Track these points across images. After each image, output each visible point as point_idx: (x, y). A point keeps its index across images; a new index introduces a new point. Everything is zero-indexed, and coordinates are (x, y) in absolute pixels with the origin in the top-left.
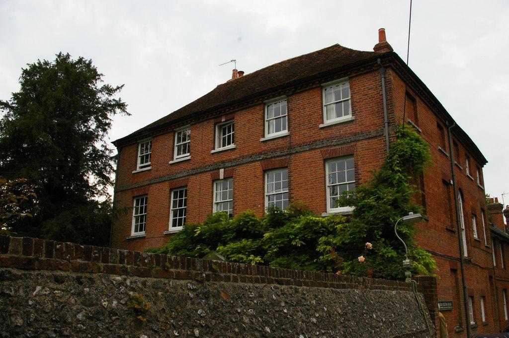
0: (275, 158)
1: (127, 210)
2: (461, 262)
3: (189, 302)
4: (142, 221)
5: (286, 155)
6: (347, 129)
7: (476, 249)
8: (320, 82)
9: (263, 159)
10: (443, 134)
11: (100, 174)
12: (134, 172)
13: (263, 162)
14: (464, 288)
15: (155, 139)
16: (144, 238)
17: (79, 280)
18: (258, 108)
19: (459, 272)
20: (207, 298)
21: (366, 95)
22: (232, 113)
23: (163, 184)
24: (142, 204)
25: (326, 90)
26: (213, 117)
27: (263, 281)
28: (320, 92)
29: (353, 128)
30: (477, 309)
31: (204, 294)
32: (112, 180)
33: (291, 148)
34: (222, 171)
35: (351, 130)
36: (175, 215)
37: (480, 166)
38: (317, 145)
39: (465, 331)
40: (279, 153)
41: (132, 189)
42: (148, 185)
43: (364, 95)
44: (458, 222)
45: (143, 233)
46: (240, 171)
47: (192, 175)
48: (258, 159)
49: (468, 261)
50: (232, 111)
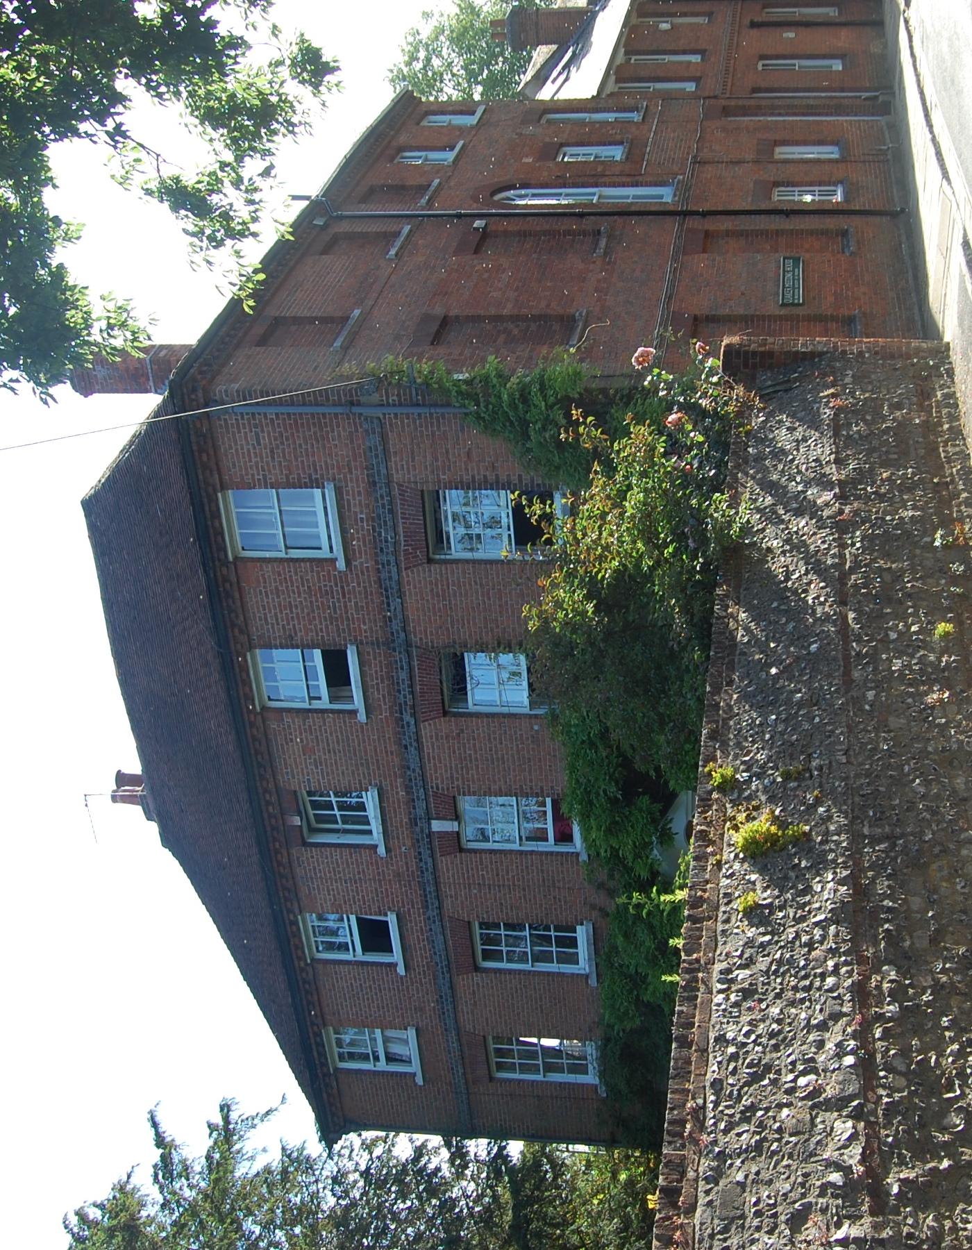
8: (225, 562)
9: (414, 715)
21: (272, 452)
34: (437, 826)
35: (359, 493)
38: (390, 578)
40: (403, 675)
41: (466, 1083)
43: (273, 458)
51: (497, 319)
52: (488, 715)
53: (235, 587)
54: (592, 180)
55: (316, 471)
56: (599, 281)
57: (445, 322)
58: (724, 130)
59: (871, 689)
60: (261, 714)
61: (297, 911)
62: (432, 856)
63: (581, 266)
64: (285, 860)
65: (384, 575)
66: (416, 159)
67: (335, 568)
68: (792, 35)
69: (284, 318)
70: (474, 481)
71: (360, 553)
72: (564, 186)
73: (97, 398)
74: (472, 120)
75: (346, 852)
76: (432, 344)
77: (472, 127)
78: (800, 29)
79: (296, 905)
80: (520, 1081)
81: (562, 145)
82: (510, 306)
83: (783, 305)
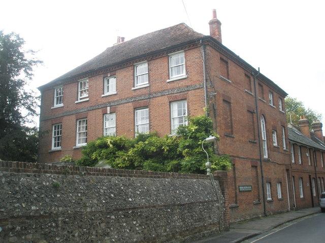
0: (142, 101)
1: (49, 132)
3: (76, 184)
4: (59, 140)
7: (275, 153)
9: (134, 101)
11: (29, 108)
12: (52, 108)
14: (263, 177)
17: (35, 176)
18: (130, 68)
19: (259, 168)
20: (84, 182)
24: (58, 129)
27: (111, 175)
29: (187, 83)
31: (83, 180)
32: (37, 112)
34: (108, 108)
36: (55, 141)
37: (282, 97)
39: (262, 204)
40: (143, 98)
44: (259, 135)
45: (59, 148)
49: (267, 161)
51: (231, 116)
57: (229, 103)
63: (246, 136)
66: (271, 97)
73: (209, 26)
74: (281, 110)
76: (248, 111)
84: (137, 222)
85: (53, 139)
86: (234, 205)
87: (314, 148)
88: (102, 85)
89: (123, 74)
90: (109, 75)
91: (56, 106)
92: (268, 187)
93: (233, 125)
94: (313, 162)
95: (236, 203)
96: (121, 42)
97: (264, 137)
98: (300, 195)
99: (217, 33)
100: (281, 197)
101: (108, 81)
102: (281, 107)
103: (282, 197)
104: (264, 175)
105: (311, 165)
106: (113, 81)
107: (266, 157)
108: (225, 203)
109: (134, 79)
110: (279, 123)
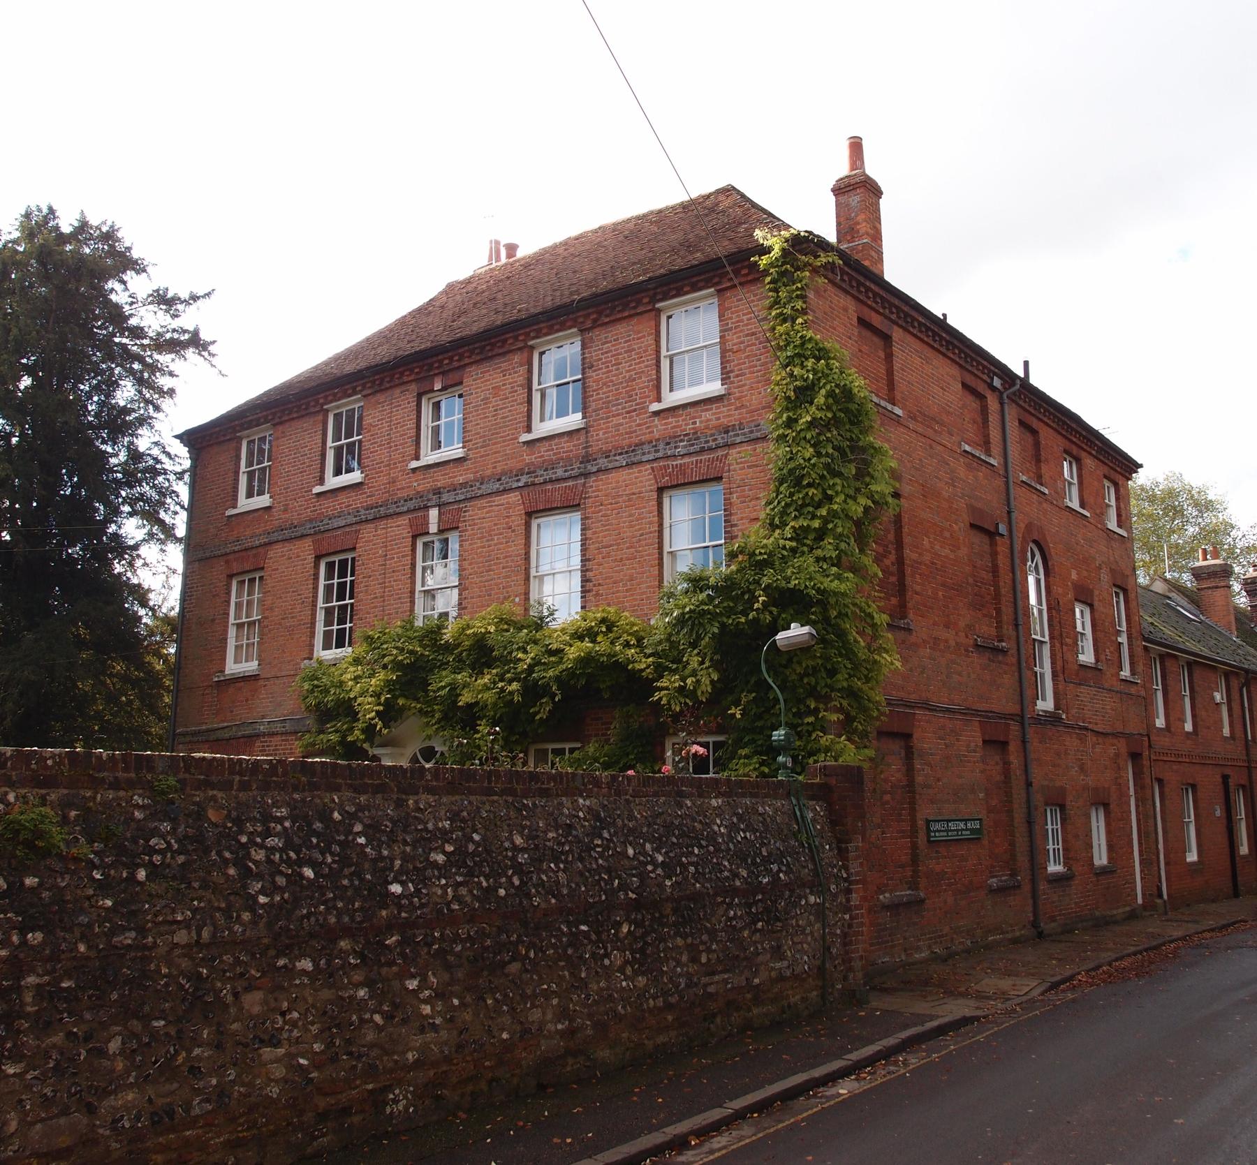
2: (1022, 724)
5: (575, 477)
6: (708, 416)
7: (1083, 689)
8: (654, 300)
9: (526, 485)
10: (984, 411)
11: (151, 516)
13: (525, 492)
14: (1029, 784)
15: (280, 428)
16: (253, 678)
18: (517, 358)
19: (1013, 747)
21: (753, 334)
22: (458, 368)
23: (298, 543)
25: (669, 317)
26: (412, 377)
28: (653, 323)
29: (725, 416)
30: (1077, 836)
33: (589, 461)
34: (434, 514)
35: (718, 419)
36: (328, 622)
37: (1121, 480)
38: (644, 454)
39: (1027, 888)
40: (560, 473)
41: (226, 554)
42: (266, 544)
43: (747, 335)
46: (474, 512)
47: (367, 521)
48: (515, 485)
49: (1052, 719)
50: (456, 364)
51: (899, 545)
52: (527, 554)
53: (633, 312)
54: (1056, 633)
55: (737, 376)
56: (946, 641)
58: (1117, 755)
59: (316, 964)
60: (526, 346)
61: (364, 393)
62: (409, 511)
63: (962, 624)
64: (405, 379)
65: (646, 448)
67: (651, 402)
68: (1218, 813)
69: (891, 347)
70: (732, 526)
71: (666, 424)
72: (1049, 609)
74: (1112, 524)
75: (413, 432)
76: (972, 525)
77: (1105, 525)
78: (1224, 821)
79: (369, 391)
80: (228, 602)
81: (1091, 606)
82: (914, 556)
83: (928, 822)
84: (424, 984)
85: (232, 632)
86: (905, 893)
87: (1247, 671)
88: (411, 424)
89: (484, 381)
90: (438, 386)
91: (245, 504)
92: (1052, 825)
93: (908, 580)
94: (1238, 728)
95: (914, 886)
96: (504, 260)
97: (1040, 630)
98: (1184, 850)
99: (863, 227)
100: (1104, 861)
101: (437, 406)
102: (1113, 513)
103: (1110, 859)
104: (1037, 775)
105: (1233, 737)
106: (453, 412)
107: (1046, 704)
108: (848, 891)
109: (530, 402)
110: (1105, 577)
